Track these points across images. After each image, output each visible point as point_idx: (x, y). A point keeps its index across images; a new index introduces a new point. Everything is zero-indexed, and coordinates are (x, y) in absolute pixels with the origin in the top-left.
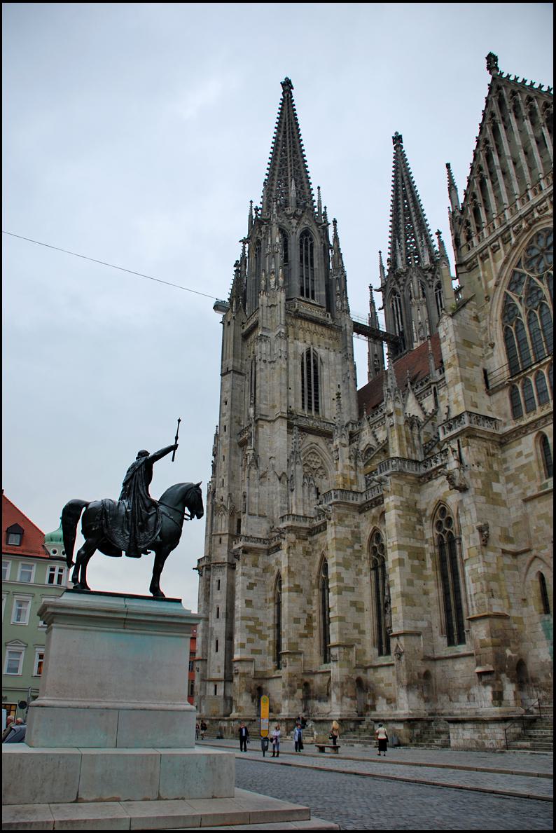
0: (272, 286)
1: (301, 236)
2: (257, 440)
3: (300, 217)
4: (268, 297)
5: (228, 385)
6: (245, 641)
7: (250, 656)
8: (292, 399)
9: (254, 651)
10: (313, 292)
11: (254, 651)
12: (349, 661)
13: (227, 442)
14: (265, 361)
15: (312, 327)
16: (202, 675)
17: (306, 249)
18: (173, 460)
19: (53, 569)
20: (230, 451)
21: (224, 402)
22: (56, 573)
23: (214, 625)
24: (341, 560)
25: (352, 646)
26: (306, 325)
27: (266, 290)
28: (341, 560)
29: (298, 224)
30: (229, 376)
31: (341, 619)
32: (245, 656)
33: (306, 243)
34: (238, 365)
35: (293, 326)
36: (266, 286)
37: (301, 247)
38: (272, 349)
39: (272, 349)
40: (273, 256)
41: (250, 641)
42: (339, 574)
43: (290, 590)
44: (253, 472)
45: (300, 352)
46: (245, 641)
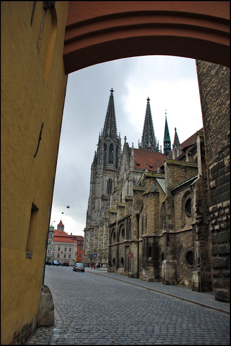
0: (101, 163)
1: (110, 146)
2: (95, 203)
3: (110, 141)
4: (99, 166)
5: (92, 186)
6: (89, 248)
7: (91, 251)
8: (104, 192)
9: (91, 250)
10: (112, 161)
11: (91, 250)
12: (100, 253)
13: (91, 201)
14: (98, 183)
15: (111, 172)
16: (84, 254)
17: (111, 149)
18: (175, 128)
19: (50, 233)
20: (91, 203)
21: (91, 191)
22: (51, 234)
23: (86, 243)
24: (100, 234)
25: (101, 251)
26: (109, 172)
27: (99, 164)
28: (100, 234)
29: (109, 143)
30: (92, 184)
31: (99, 246)
32: (89, 251)
33: (112, 147)
34: (94, 181)
35: (106, 173)
36: (99, 163)
37: (110, 149)
38: (99, 180)
39: (99, 180)
40: (102, 154)
41: (91, 248)
42: (100, 237)
43: (95, 238)
44: (93, 211)
45: (107, 180)
46: (89, 248)
